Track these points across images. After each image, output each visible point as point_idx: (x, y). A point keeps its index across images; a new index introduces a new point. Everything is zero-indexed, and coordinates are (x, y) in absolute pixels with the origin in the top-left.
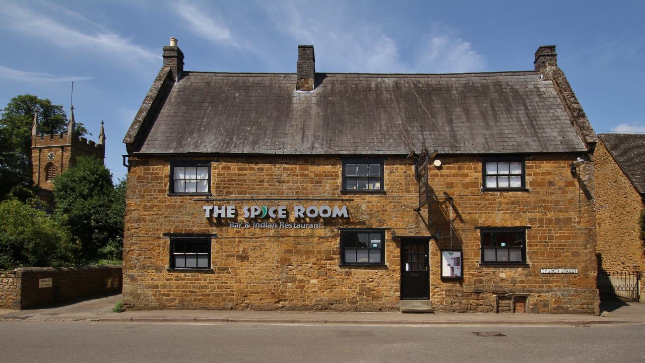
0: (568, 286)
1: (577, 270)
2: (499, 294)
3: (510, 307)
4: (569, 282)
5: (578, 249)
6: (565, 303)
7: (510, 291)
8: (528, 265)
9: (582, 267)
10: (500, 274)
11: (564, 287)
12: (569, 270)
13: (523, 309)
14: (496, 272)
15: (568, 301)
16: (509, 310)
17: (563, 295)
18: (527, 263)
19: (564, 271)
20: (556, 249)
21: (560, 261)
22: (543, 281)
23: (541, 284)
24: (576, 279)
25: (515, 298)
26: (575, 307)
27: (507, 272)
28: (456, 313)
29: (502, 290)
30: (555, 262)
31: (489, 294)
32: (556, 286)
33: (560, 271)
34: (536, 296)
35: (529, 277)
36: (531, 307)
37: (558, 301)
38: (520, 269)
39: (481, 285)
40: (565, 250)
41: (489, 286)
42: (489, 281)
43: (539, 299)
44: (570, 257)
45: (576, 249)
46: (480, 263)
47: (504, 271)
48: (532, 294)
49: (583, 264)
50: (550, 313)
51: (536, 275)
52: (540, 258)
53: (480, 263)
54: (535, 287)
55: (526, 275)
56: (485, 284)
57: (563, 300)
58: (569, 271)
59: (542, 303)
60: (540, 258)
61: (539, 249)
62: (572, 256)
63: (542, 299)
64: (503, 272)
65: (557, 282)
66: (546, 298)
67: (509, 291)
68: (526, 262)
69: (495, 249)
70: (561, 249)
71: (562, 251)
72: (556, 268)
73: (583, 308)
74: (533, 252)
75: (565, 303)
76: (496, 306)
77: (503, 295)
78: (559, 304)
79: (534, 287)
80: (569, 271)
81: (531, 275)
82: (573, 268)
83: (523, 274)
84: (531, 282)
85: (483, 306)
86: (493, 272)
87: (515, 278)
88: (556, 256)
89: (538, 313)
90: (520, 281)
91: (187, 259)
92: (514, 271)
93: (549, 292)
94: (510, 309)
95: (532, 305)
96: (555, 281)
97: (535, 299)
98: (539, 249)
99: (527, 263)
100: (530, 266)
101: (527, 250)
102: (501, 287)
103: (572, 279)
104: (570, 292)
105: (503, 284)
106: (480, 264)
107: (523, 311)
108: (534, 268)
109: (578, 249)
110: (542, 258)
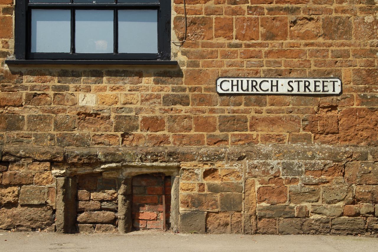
0: (307, 138)
1: (338, 84)
2: (74, 164)
3: (116, 211)
4: (311, 125)
5: (344, 11)
6: (298, 195)
7: (112, 157)
8: (175, 63)
9: (358, 72)
10: (80, 96)
11: (294, 140)
12: (312, 81)
13: (162, 216)
14: (67, 89)
15: (307, 188)
16: (114, 222)
17: (287, 167)
18: (173, 59)
19: (295, 85)
20: (270, 10)
21: (281, 53)
22: (224, 120)
23: (217, 133)
24: (334, 113)
25: (131, 181)
26: (330, 210)
27: (104, 89)
28: (310, 235)
29: (85, 151)
30: (268, 54)
31: (37, 167)
32: (267, 139)
33: (283, 85)
34: (200, 172)
35: (178, 107)
36: (182, 209)
37: (272, 191)
38: (148, 82)
39: (14, 134)
40: (302, 15)
41: (39, 139)
42: (42, 119)
43: (209, 181)
44: (317, 36)
45: (336, 11)
46: (12, 57)
47: (93, 86)
48: (184, 165)
49: (360, 63)
50: (246, 232)
51: (202, 100)
52: (214, 41)
53: (12, 57)
54: (199, 141)
55: (168, 100)
56: (25, 131)
57: (290, 187)
58: (312, 87)
59: (218, 196)
60: (214, 41)
61: (214, 12)
62: (324, 35)
63: (217, 182)
64: (88, 90)
65: (273, 122)
66: (232, 179)
67: (106, 155)
68: (169, 58)
69: (68, 13)
70: (287, 10)
71: (292, 17)
72: (269, 74)
73: (358, 214)
74: (193, 22)
75: (298, 195)
76: (60, 208)
77: (88, 170)
78: (274, 200)
79: (192, 141)
80: (312, 87)
81: (184, 101)
82: (326, 75)
83: (158, 97)
84: (185, 123)
85: (19, 209)
86: (55, 88)
87: (131, 110)
88: (270, 36)
89: (206, 230)
90: (145, 120)
91: (111, 51)
92: (128, 87)
93: (241, 158)
94: (116, 219)
95: (186, 203)
96: (264, 120)
97: (194, 183)
98: (214, 12)
99: (173, 59)
100: (184, 68)
101: (174, 14)
102: (81, 141)
103: (323, 113)
104: (313, 157)
105: (87, 131)
106: (8, 63)
107: (161, 223)
108: (194, 77)
109: (344, 11)
110: (222, 40)
